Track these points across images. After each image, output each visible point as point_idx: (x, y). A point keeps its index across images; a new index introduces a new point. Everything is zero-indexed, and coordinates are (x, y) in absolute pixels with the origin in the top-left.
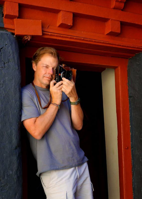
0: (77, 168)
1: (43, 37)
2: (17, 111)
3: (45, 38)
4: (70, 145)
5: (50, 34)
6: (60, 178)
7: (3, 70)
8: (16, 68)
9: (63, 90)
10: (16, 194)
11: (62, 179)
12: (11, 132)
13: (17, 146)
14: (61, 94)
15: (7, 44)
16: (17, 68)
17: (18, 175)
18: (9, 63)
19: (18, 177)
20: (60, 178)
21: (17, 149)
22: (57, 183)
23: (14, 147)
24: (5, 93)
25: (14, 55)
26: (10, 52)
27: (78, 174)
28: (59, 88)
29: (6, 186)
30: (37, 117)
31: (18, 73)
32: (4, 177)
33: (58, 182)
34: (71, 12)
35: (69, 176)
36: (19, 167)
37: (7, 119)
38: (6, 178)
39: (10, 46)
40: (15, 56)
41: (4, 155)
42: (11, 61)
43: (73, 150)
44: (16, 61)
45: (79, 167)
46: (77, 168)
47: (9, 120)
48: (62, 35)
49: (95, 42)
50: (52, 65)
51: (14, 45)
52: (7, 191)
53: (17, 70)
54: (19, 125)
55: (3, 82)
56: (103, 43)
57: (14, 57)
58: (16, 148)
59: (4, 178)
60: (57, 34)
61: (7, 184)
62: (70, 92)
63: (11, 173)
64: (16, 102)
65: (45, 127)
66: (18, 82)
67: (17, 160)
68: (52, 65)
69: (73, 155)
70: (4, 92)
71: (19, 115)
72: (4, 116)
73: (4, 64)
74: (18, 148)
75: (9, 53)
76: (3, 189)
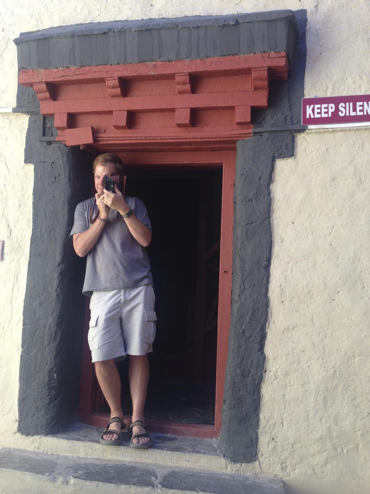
0: (122, 291)
1: (98, 143)
2: (63, 227)
3: (101, 144)
4: (115, 264)
5: (104, 139)
6: (99, 300)
7: (53, 185)
8: (66, 182)
9: (105, 202)
10: (53, 312)
11: (100, 301)
12: (55, 248)
13: (60, 263)
14: (103, 207)
15: (58, 157)
16: (67, 181)
17: (57, 292)
18: (60, 177)
19: (58, 295)
20: (99, 300)
21: (61, 265)
22: (95, 305)
23: (57, 263)
24: (53, 208)
25: (64, 167)
26: (61, 165)
27: (122, 298)
28: (102, 201)
29: (45, 302)
30: (81, 233)
31: (68, 187)
32: (44, 293)
33: (96, 304)
34: (125, 110)
35: (107, 299)
36: (60, 284)
37: (53, 235)
38: (45, 294)
39: (62, 159)
40: (66, 169)
41: (47, 271)
42: (61, 175)
43: (118, 270)
44: (67, 175)
45: (128, 291)
46: (122, 291)
47: (54, 236)
48: (119, 138)
49: (160, 139)
50: (102, 174)
51: (65, 157)
52: (45, 308)
53: (67, 183)
54: (65, 241)
55: (52, 197)
56: (172, 139)
57: (64, 171)
58: (59, 265)
59: (43, 294)
60: (113, 138)
61: (46, 301)
62: (111, 204)
63: (51, 290)
64: (64, 218)
65: (85, 243)
66: (68, 196)
67: (58, 277)
68: (102, 174)
69: (118, 276)
70: (52, 208)
71: (66, 231)
72: (50, 231)
73: (55, 178)
74: (62, 265)
75: (60, 166)
76: (41, 305)
